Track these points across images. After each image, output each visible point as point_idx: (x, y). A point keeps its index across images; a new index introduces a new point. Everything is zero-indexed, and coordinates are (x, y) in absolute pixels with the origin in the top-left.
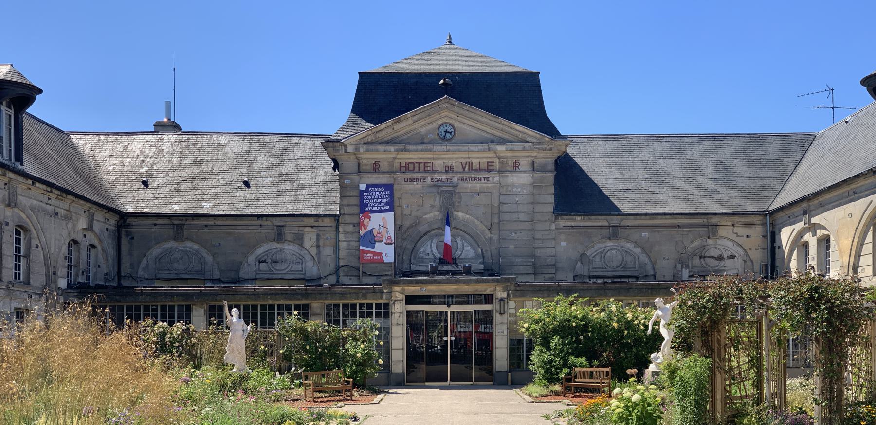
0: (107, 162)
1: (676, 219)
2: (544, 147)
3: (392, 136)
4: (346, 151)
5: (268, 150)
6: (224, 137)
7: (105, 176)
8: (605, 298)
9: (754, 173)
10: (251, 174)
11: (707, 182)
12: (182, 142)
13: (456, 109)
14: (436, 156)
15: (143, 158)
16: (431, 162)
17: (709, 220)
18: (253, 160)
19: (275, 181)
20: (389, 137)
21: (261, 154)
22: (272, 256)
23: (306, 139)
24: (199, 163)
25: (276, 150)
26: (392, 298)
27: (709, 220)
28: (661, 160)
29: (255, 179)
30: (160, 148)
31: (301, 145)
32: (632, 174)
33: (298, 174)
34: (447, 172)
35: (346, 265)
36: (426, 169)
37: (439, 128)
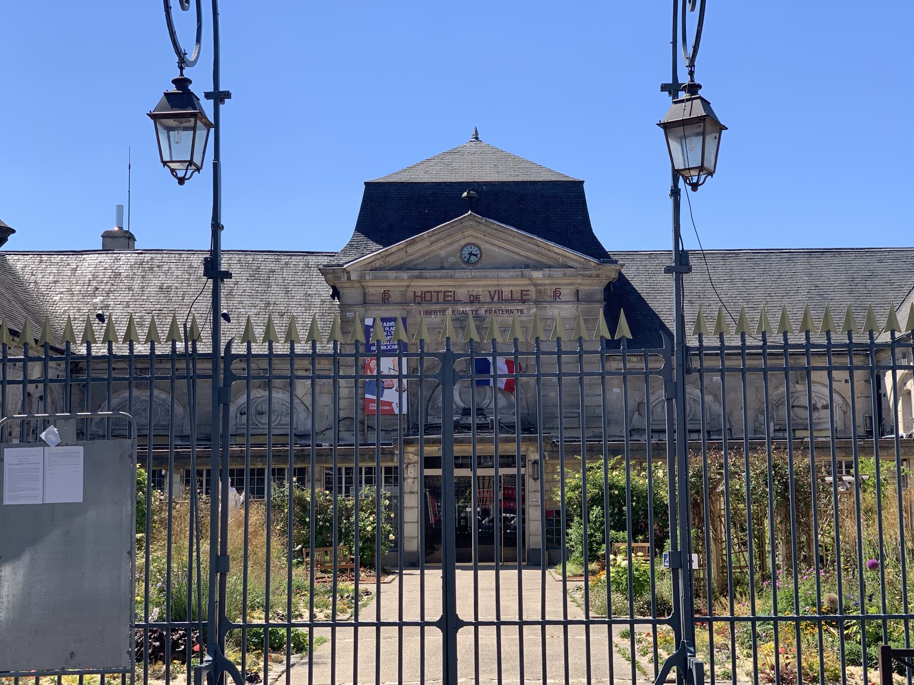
0: (52, 290)
1: (755, 359)
2: (589, 273)
3: (405, 260)
4: (349, 279)
5: (251, 273)
6: (196, 256)
7: (51, 308)
8: (659, 460)
9: (856, 300)
10: (231, 304)
11: (796, 312)
12: (144, 263)
13: (482, 228)
14: (459, 283)
15: (96, 284)
16: (453, 290)
17: (797, 361)
18: (233, 286)
19: (261, 313)
20: (402, 262)
21: (243, 278)
22: (257, 406)
23: (297, 258)
24: (166, 290)
25: (260, 273)
26: (405, 461)
27: (797, 361)
28: (739, 284)
29: (237, 310)
30: (117, 271)
31: (291, 266)
32: (701, 302)
33: (288, 303)
34: (472, 302)
35: (348, 418)
36: (446, 299)
37: (462, 250)
